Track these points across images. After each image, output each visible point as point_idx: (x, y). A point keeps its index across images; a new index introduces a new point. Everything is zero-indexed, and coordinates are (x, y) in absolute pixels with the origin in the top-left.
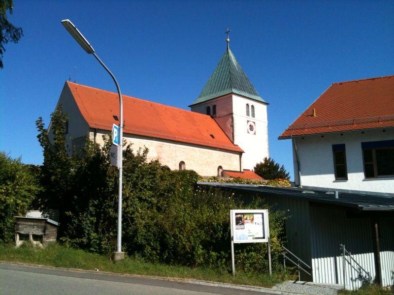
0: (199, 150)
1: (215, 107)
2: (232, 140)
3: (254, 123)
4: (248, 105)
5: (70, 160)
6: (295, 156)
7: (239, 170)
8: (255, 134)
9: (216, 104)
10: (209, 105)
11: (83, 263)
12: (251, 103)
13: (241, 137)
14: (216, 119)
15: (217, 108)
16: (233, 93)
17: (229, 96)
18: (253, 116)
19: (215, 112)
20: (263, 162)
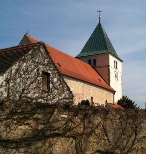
0: (95, 88)
1: (95, 60)
2: (108, 83)
3: (117, 73)
4: (115, 61)
5: (89, 112)
6: (113, 90)
7: (113, 103)
8: (117, 80)
9: (95, 58)
10: (90, 58)
11: (29, 130)
12: (116, 60)
13: (114, 84)
14: (97, 69)
15: (97, 61)
16: (109, 53)
17: (106, 54)
18: (117, 69)
19: (95, 64)
20: (121, 98)
